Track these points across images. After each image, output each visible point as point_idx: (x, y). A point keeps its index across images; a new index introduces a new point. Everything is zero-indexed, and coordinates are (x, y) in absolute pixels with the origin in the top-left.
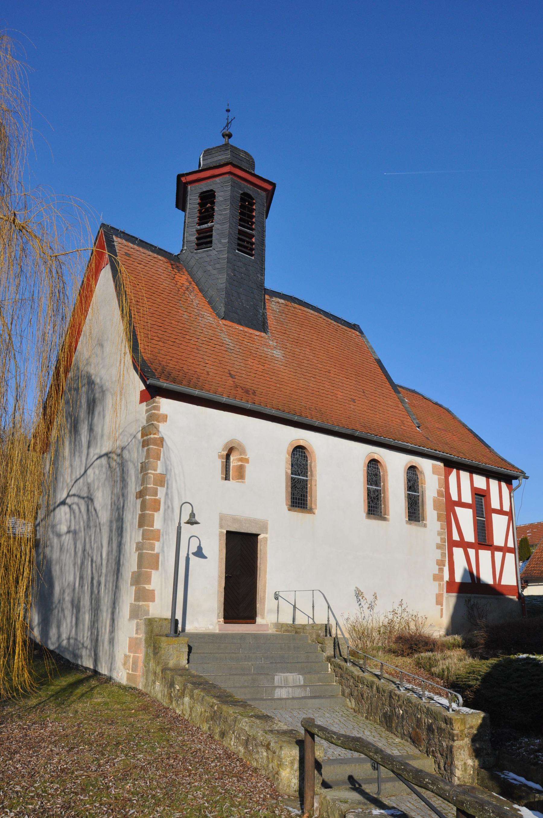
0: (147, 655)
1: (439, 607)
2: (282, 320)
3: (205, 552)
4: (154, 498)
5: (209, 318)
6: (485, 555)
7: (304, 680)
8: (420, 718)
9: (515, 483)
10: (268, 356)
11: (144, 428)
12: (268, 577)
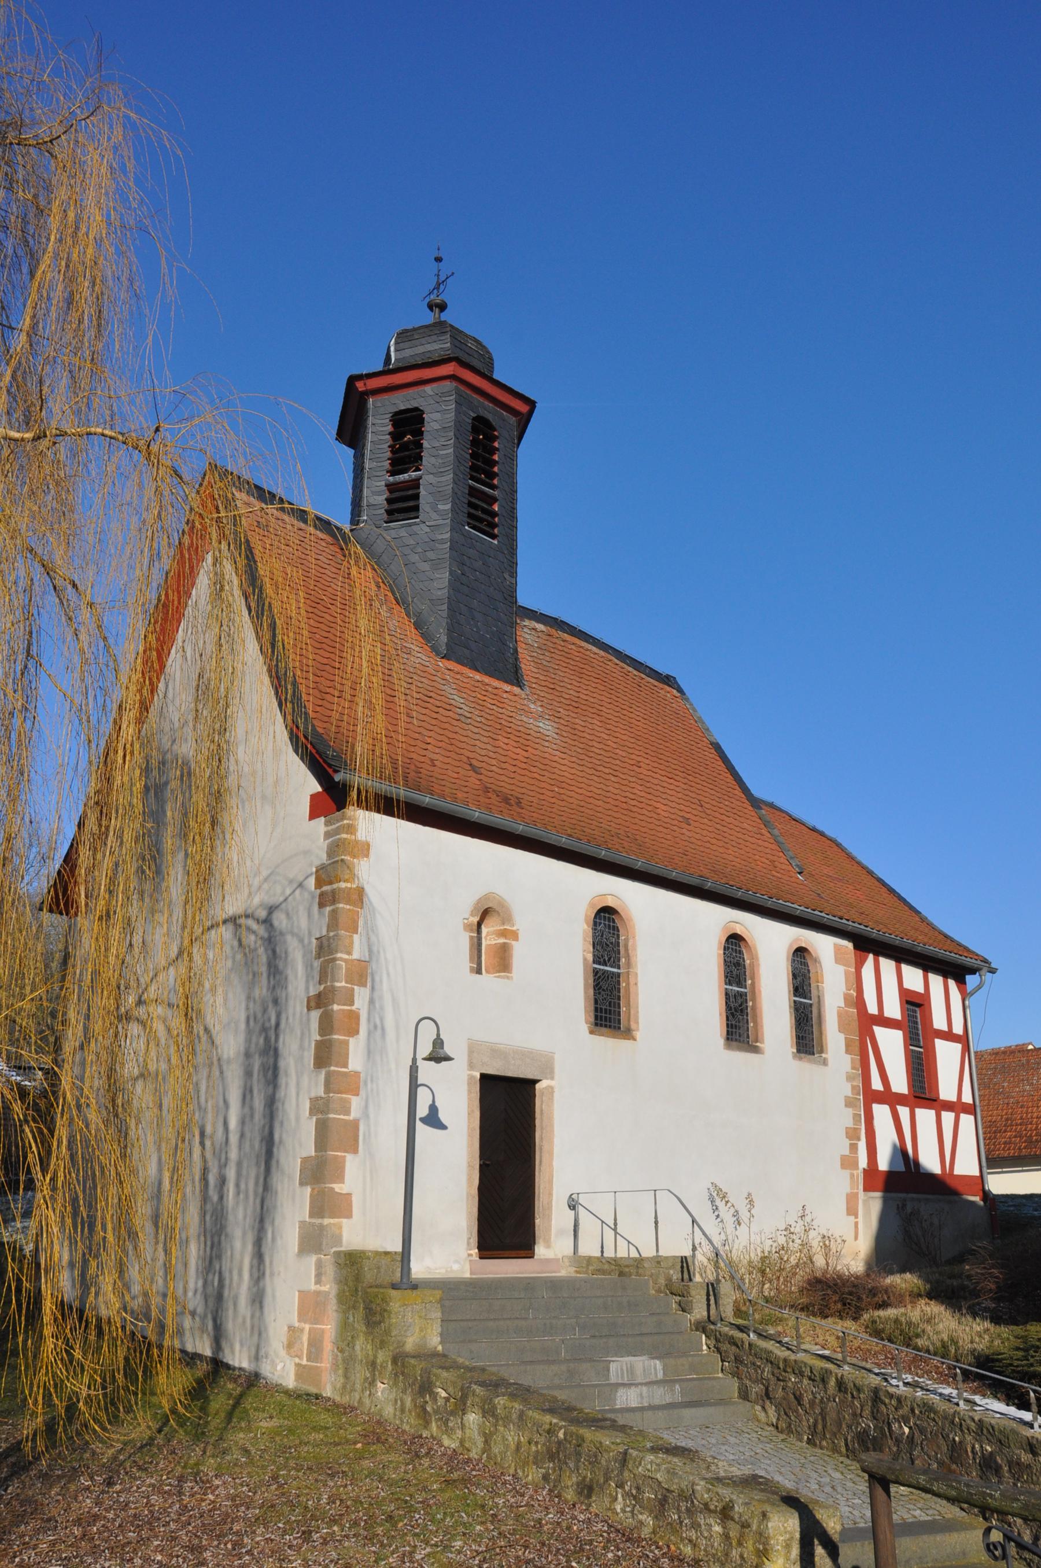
0: (344, 1326)
1: (852, 1218)
2: (545, 663)
3: (443, 1116)
4: (349, 1008)
5: (419, 655)
6: (926, 1116)
7: (663, 1369)
8: (960, 1442)
9: (971, 980)
10: (531, 732)
11: (321, 870)
12: (555, 1164)
